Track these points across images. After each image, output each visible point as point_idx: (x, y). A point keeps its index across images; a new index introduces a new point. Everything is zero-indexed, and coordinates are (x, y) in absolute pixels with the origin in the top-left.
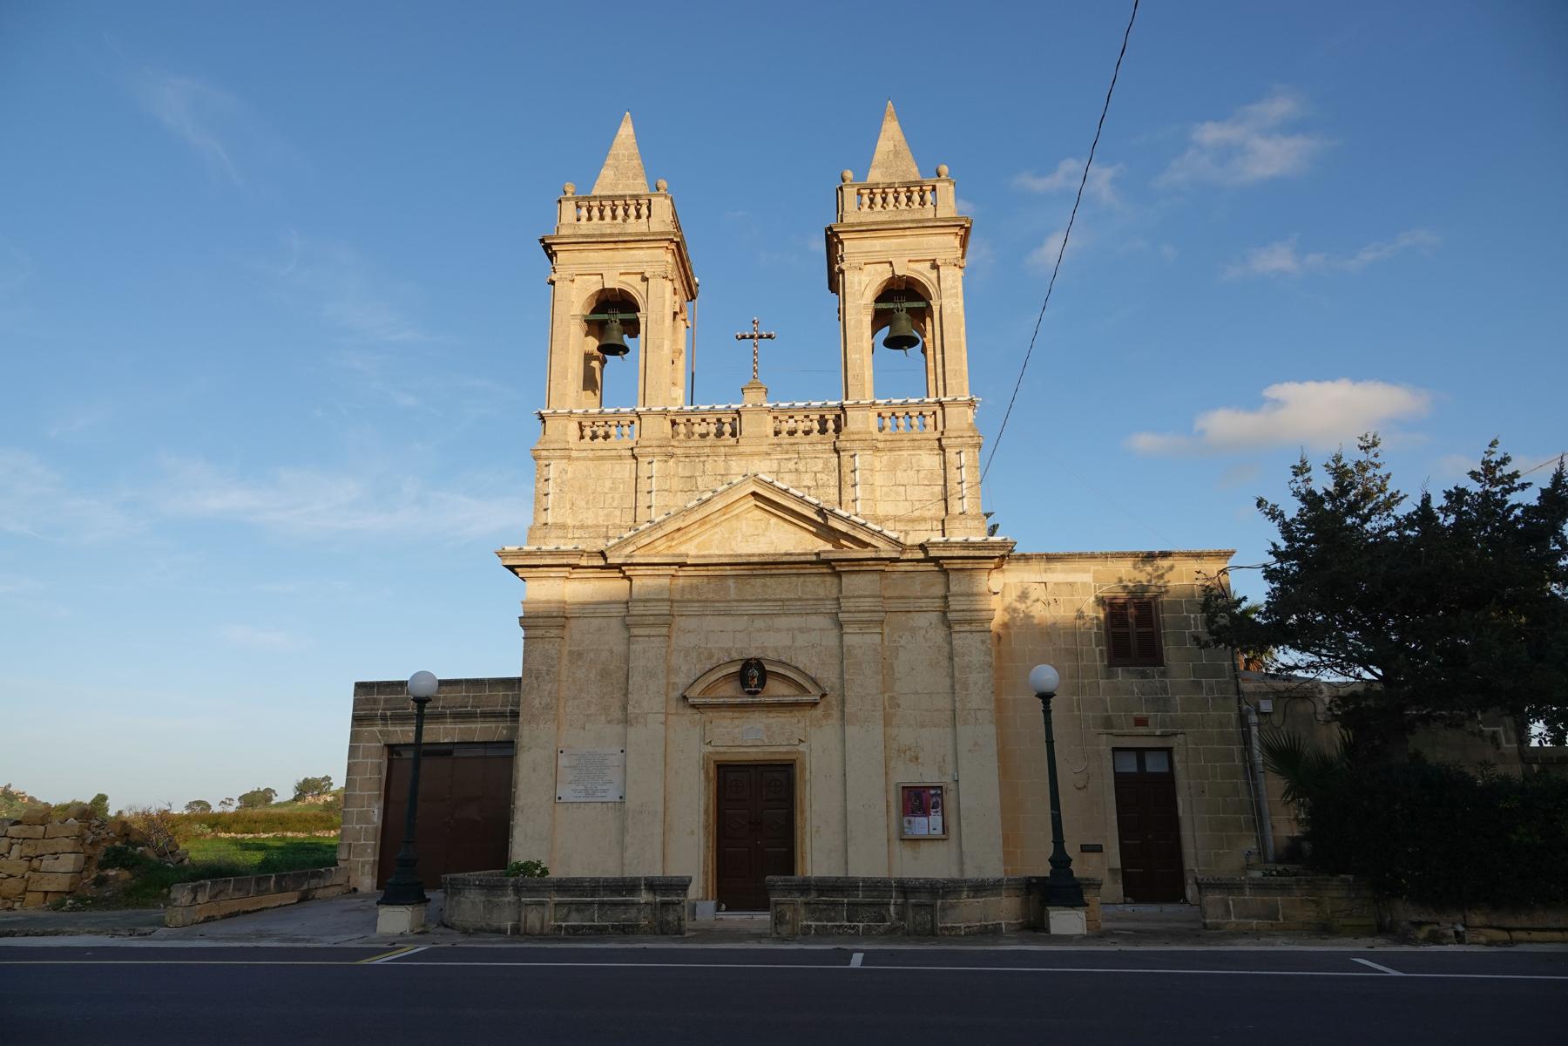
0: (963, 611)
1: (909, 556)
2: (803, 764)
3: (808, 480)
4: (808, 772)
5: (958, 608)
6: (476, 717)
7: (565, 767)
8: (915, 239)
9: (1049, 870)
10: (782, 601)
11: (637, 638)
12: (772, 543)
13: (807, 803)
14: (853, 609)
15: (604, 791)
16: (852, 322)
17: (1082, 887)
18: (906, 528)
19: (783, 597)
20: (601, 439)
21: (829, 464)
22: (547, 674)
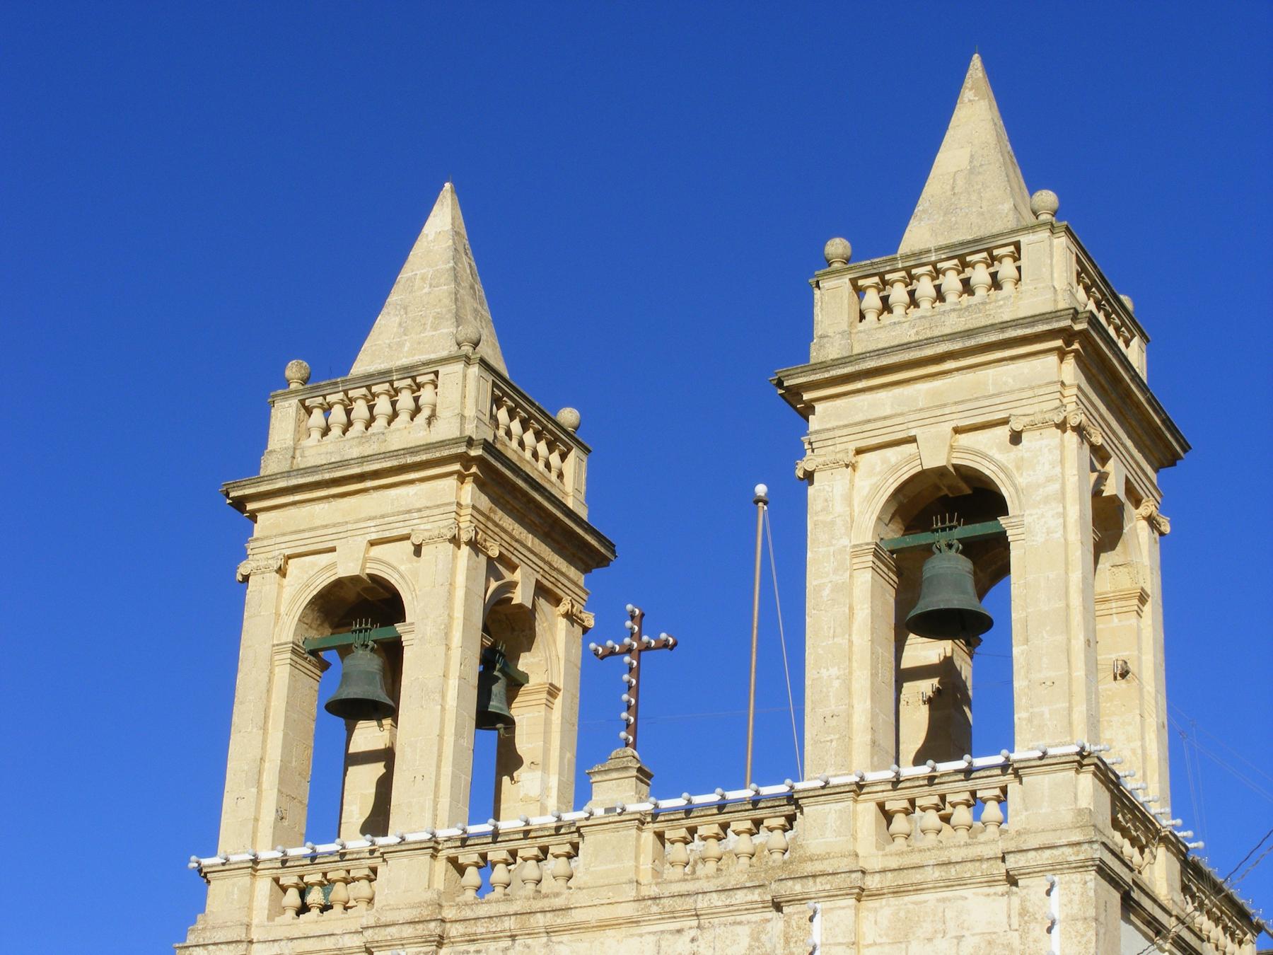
8: (970, 376)
16: (826, 592)
21: (763, 937)
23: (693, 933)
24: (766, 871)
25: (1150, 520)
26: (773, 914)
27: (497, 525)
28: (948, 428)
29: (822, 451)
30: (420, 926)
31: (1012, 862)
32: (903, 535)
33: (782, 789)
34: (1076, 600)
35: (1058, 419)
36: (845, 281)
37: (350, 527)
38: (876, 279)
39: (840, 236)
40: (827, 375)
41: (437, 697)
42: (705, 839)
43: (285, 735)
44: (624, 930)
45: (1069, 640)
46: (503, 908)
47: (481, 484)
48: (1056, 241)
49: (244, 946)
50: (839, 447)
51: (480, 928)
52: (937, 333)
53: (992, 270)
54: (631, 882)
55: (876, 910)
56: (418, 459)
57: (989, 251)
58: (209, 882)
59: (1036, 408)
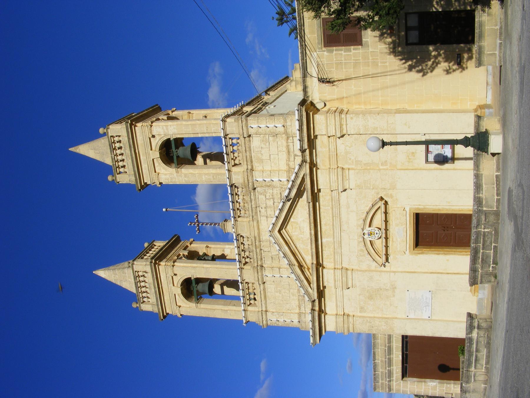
0: (335, 129)
1: (308, 158)
2: (416, 209)
3: (270, 203)
4: (420, 207)
5: (334, 131)
6: (390, 345)
7: (415, 315)
9: (471, 148)
10: (333, 217)
11: (353, 284)
12: (304, 220)
13: (434, 207)
14: (336, 184)
15: (426, 298)
17: (479, 132)
18: (293, 156)
19: (331, 215)
20: (255, 296)
21: (261, 192)
22: (371, 323)
23: (260, 208)
24: (247, 192)
25: (172, 112)
26: (256, 190)
27: (170, 257)
28: (151, 152)
29: (155, 180)
30: (259, 271)
31: (245, 136)
32: (174, 163)
33: (229, 188)
34: (189, 123)
35: (150, 127)
36: (118, 176)
37: (170, 291)
38: (117, 169)
39: (108, 177)
40: (138, 179)
41: (208, 269)
42: (238, 191)
43: (216, 305)
44: (260, 224)
45: (198, 124)
46: (255, 252)
47: (161, 261)
48: (111, 128)
49: (263, 312)
50: (154, 177)
51: (259, 257)
52: (130, 155)
53: (119, 155)
54: (249, 223)
55: (256, 167)
56: (155, 275)
57: (112, 143)
58: (249, 321)
59: (147, 132)
